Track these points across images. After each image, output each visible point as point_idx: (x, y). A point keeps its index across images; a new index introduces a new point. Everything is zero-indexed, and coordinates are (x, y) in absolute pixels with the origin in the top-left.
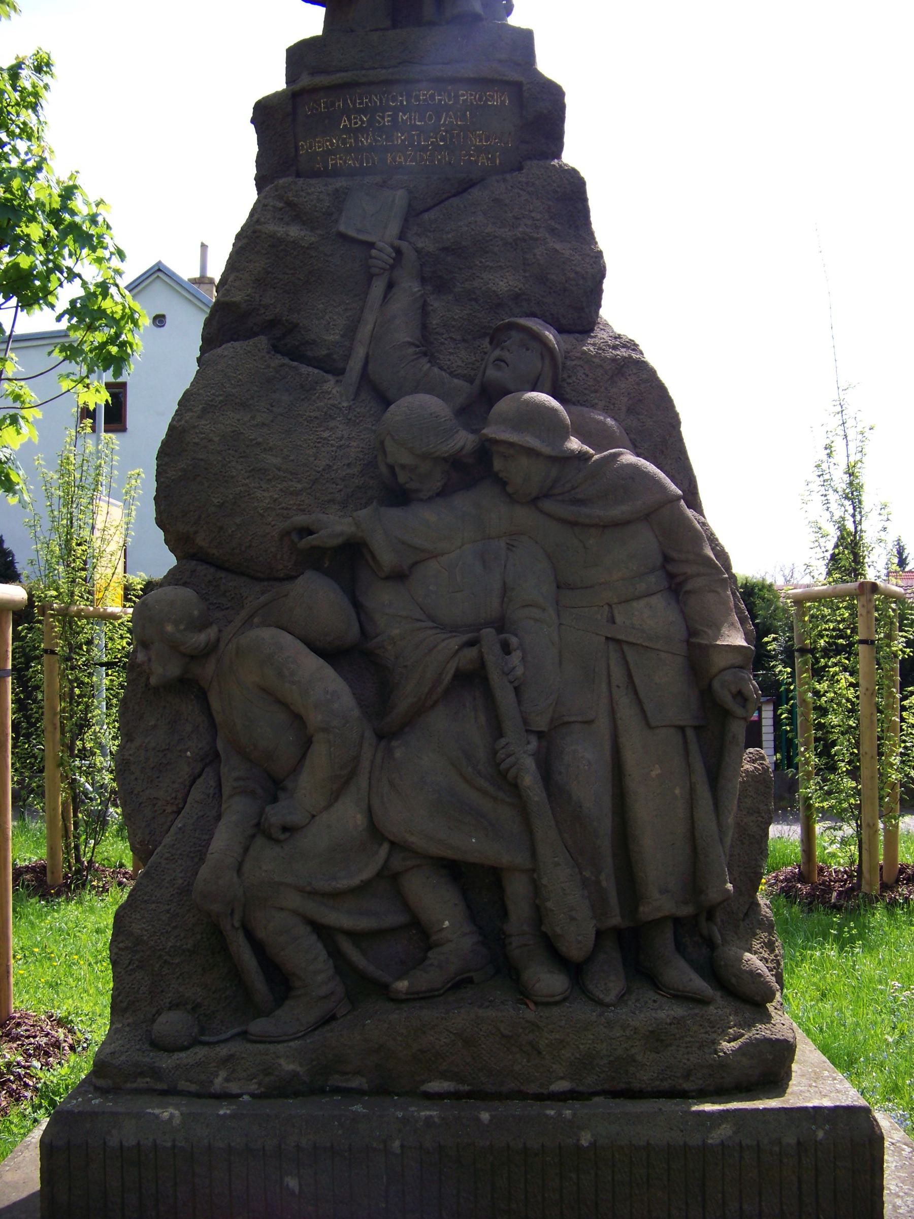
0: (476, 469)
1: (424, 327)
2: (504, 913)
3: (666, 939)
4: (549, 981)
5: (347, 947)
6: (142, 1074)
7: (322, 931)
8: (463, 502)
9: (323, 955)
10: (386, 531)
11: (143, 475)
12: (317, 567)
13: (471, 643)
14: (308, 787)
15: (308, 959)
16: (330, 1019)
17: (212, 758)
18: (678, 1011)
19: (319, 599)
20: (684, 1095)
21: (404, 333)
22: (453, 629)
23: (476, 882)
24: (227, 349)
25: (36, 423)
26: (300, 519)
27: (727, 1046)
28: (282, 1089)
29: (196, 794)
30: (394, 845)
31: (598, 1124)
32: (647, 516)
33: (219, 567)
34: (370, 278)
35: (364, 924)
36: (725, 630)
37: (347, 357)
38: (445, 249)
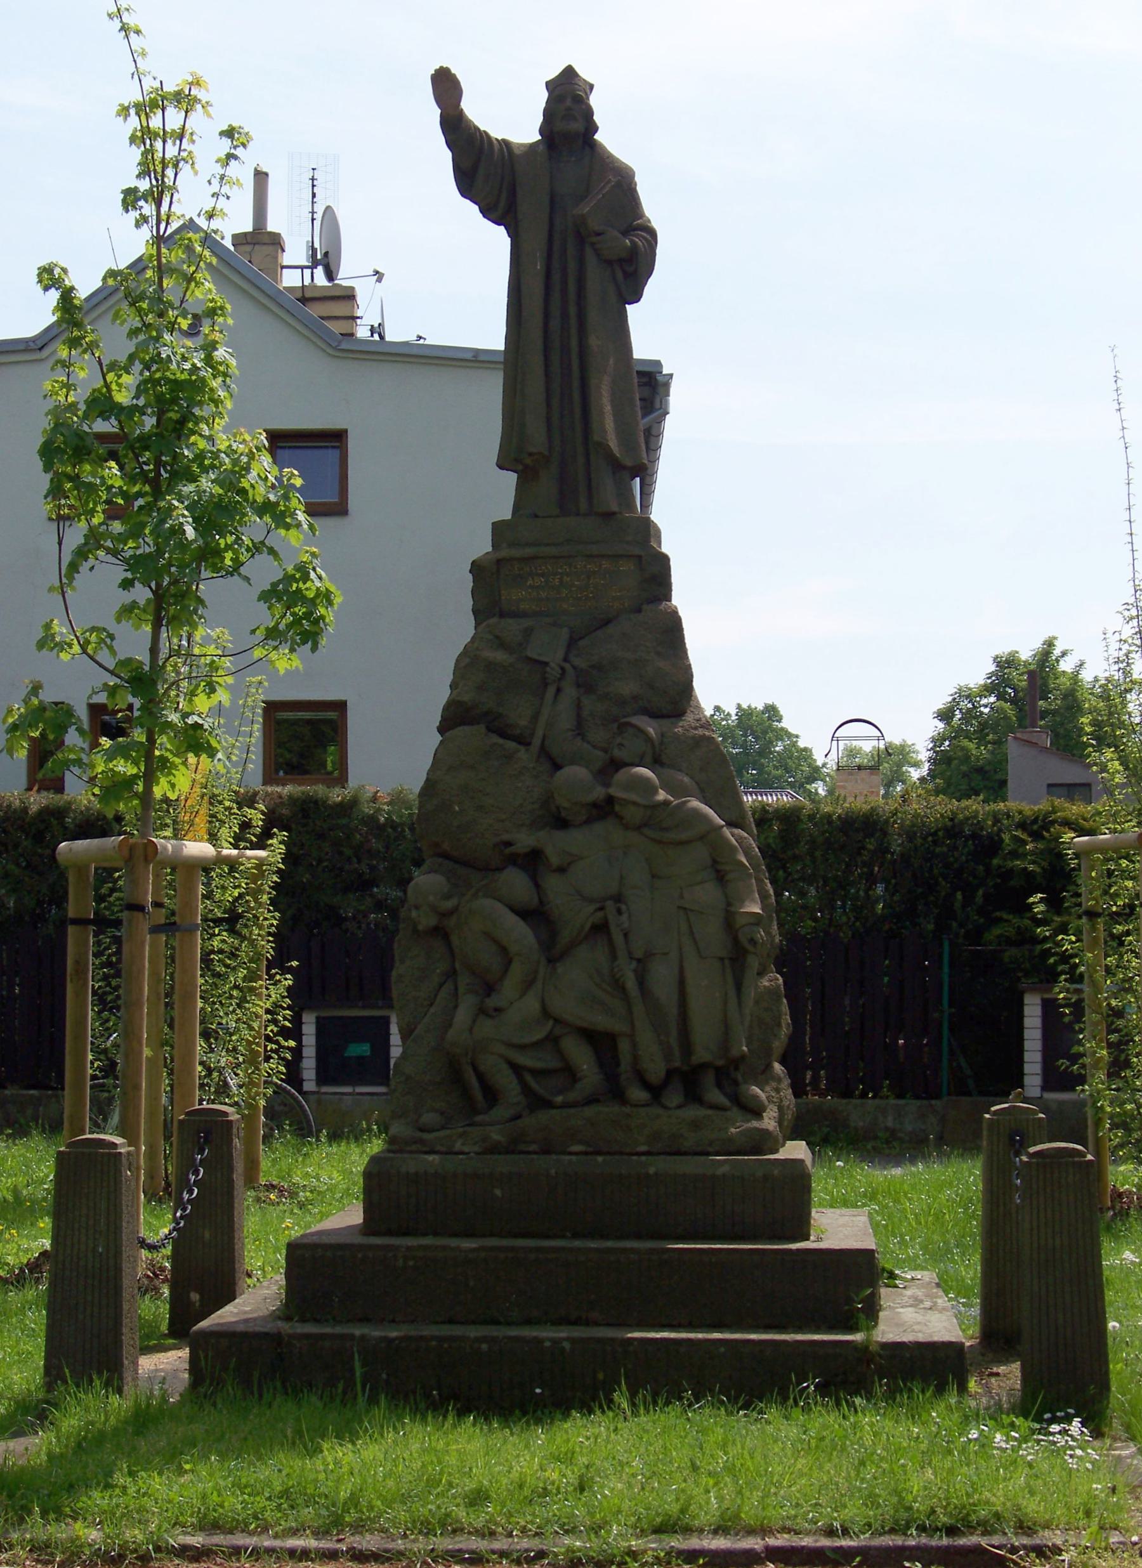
0: (605, 809)
1: (579, 716)
2: (618, 1064)
3: (709, 1079)
4: (637, 1094)
5: (529, 1078)
6: (415, 1143)
7: (516, 1068)
8: (599, 828)
9: (515, 1081)
10: (555, 844)
11: (266, 684)
12: (515, 864)
13: (601, 909)
14: (509, 988)
15: (506, 1081)
16: (518, 1117)
17: (452, 974)
18: (709, 1112)
19: (515, 882)
20: (708, 1154)
21: (566, 721)
22: (591, 900)
23: (602, 1043)
24: (460, 731)
25: (228, 687)
26: (506, 837)
27: (733, 1130)
28: (493, 1149)
29: (443, 993)
30: (556, 1020)
31: (657, 1165)
32: (702, 838)
33: (457, 862)
34: (546, 685)
35: (539, 1065)
36: (747, 903)
37: (532, 735)
38: (593, 667)
